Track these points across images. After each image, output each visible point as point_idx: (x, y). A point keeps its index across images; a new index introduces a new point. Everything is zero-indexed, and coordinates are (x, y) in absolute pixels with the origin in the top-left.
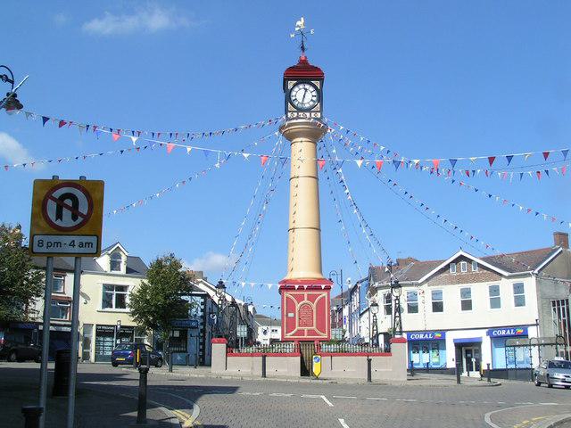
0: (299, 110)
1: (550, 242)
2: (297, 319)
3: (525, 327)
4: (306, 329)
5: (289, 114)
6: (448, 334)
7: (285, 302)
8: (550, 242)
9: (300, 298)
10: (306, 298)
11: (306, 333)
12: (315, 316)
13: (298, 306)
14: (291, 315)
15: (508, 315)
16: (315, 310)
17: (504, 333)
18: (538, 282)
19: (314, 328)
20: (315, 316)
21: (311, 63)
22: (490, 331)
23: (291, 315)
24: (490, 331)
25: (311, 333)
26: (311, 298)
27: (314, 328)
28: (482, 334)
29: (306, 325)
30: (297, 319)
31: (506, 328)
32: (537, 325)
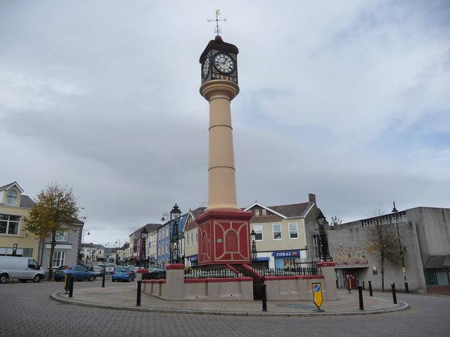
0: (221, 73)
1: (307, 200)
2: (225, 244)
3: (298, 251)
4: (232, 253)
5: (213, 75)
6: (301, 252)
7: (61, 256)
8: (307, 200)
9: (227, 226)
10: (231, 227)
11: (232, 258)
12: (238, 241)
13: (225, 233)
14: (220, 241)
15: (286, 244)
16: (238, 238)
17: (284, 254)
18: (306, 223)
19: (239, 252)
20: (238, 241)
21: (225, 40)
22: (275, 253)
23: (220, 241)
24: (275, 253)
25: (236, 256)
26: (236, 226)
27: (239, 252)
28: (269, 255)
29: (231, 250)
30: (225, 244)
31: (285, 251)
32: (306, 249)
